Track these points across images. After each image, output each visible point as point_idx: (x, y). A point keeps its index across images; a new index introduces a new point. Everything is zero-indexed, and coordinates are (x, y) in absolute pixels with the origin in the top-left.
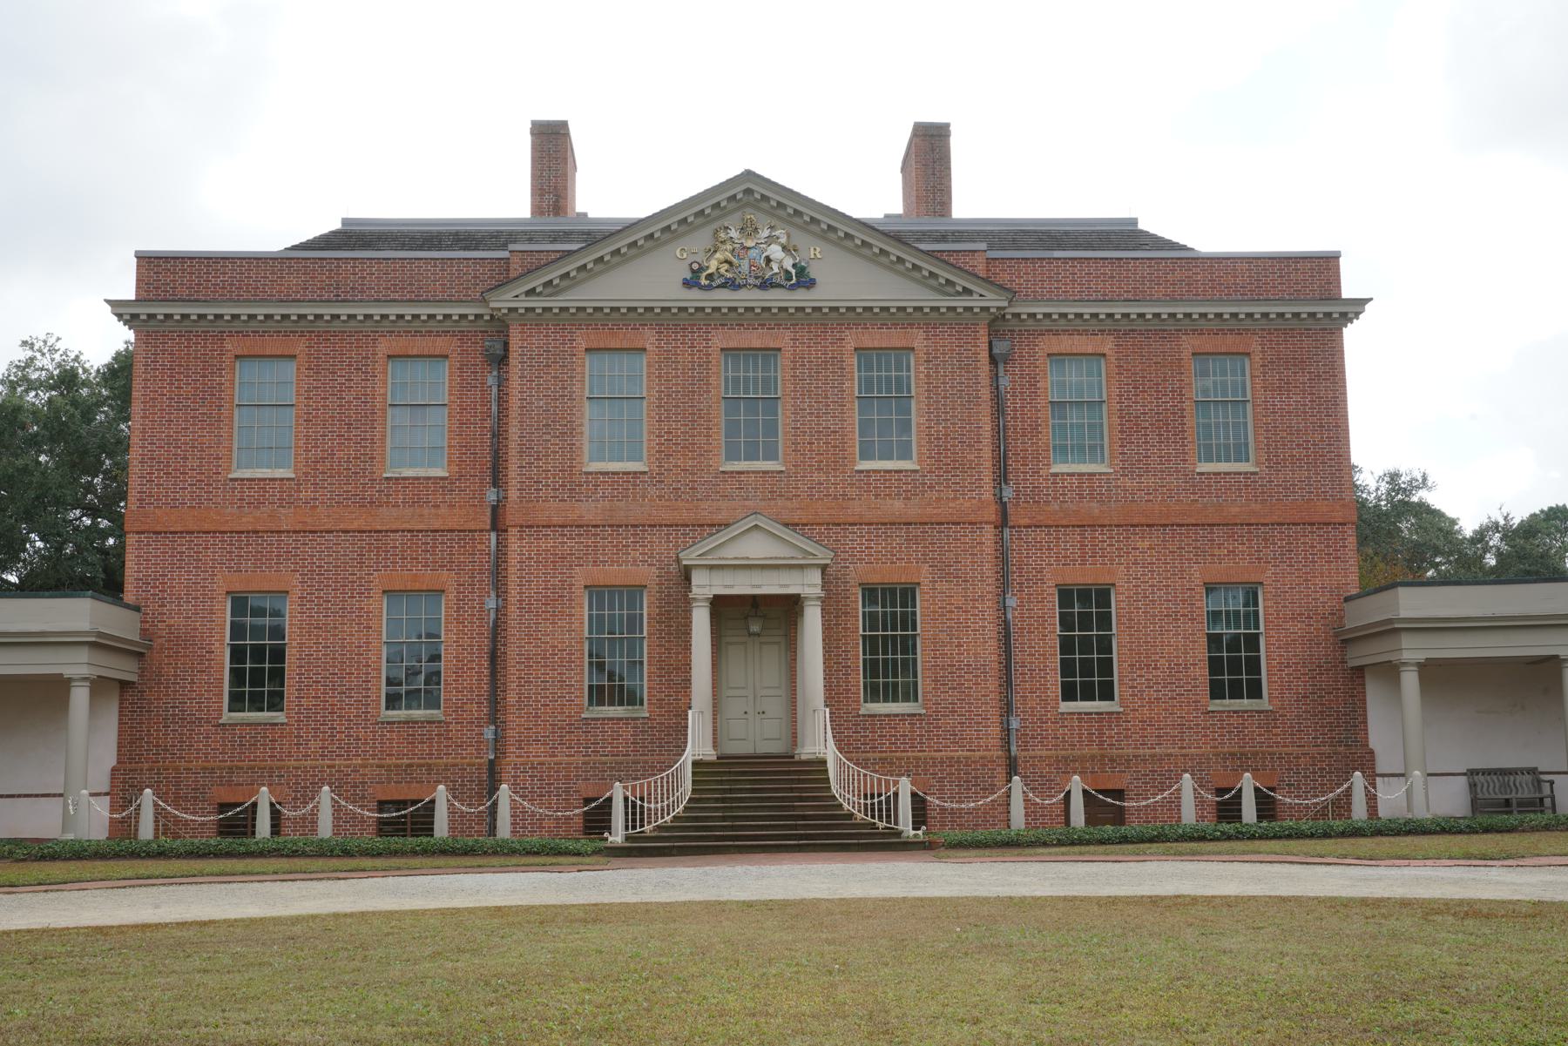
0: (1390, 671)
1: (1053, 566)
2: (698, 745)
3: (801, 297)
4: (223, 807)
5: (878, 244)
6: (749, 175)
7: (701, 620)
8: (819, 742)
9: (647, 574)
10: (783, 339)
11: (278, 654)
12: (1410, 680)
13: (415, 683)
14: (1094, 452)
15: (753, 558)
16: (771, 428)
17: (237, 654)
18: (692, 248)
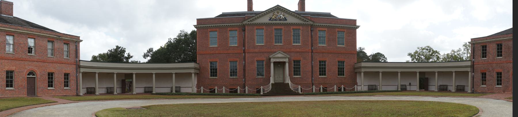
0: (360, 73)
1: (318, 58)
2: (272, 81)
3: (285, 22)
4: (210, 89)
5: (296, 15)
6: (278, 5)
7: (272, 65)
8: (288, 81)
9: (265, 59)
10: (283, 27)
11: (216, 69)
12: (362, 74)
13: (234, 73)
14: (324, 43)
15: (279, 56)
16: (281, 39)
17: (211, 70)
18: (271, 15)
